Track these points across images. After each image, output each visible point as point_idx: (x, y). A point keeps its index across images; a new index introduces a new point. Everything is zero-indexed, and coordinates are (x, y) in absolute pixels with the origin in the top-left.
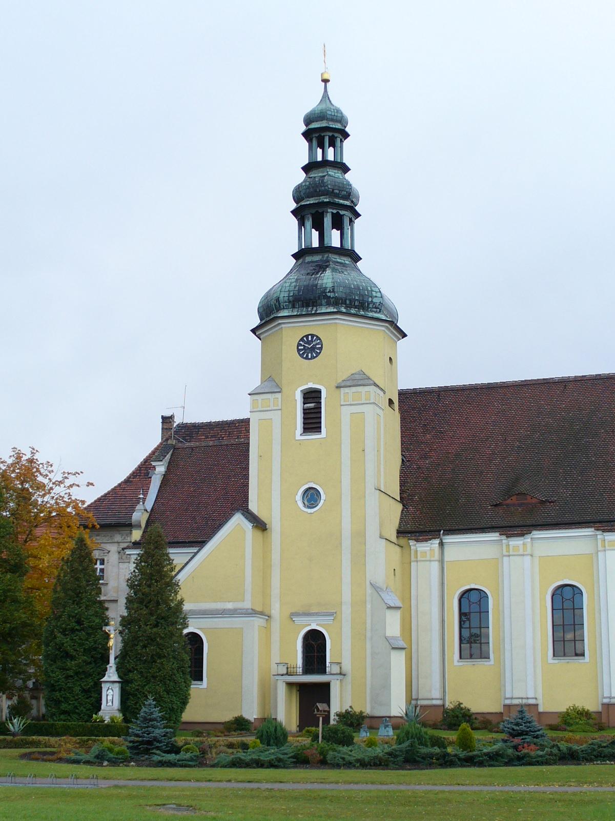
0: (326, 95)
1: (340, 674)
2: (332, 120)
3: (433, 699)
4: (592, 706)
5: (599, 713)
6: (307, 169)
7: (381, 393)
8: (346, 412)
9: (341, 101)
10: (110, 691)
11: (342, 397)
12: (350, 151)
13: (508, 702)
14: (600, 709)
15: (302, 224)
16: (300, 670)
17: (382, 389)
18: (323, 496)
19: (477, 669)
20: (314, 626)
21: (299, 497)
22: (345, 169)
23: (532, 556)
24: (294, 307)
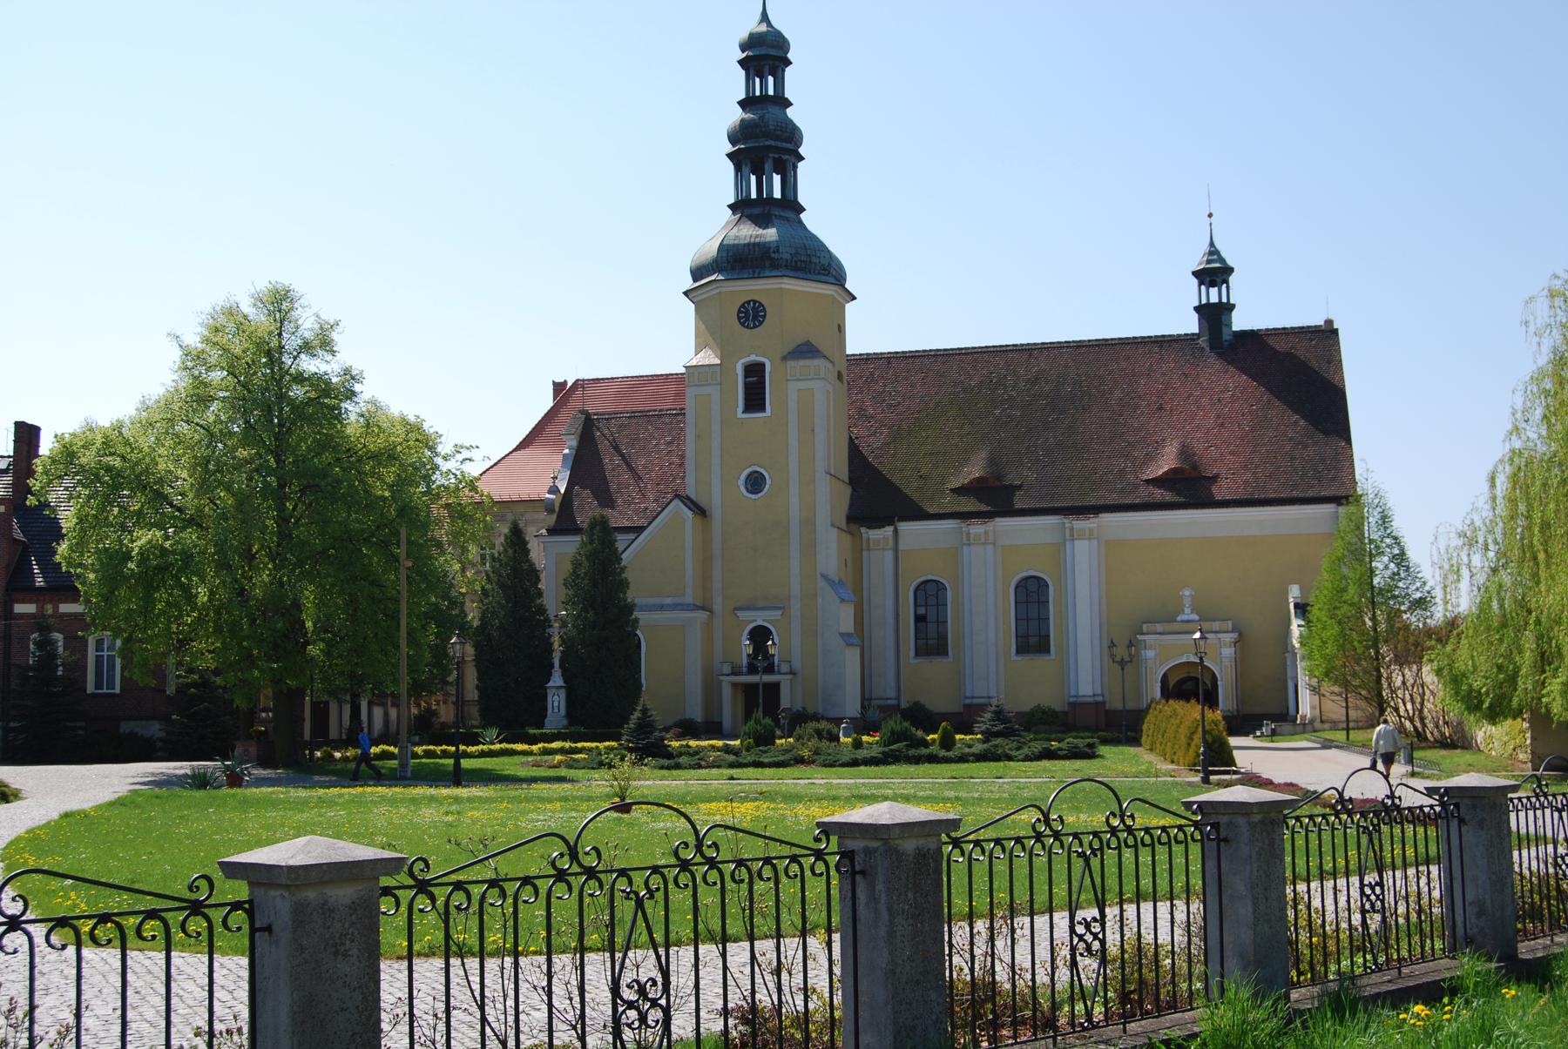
1: (791, 673)
2: (773, 46)
3: (887, 699)
4: (1057, 705)
5: (1065, 713)
7: (830, 366)
8: (793, 387)
10: (556, 697)
12: (795, 82)
14: (1066, 709)
15: (738, 169)
16: (745, 670)
17: (831, 362)
18: (768, 482)
19: (935, 669)
21: (741, 482)
23: (994, 544)
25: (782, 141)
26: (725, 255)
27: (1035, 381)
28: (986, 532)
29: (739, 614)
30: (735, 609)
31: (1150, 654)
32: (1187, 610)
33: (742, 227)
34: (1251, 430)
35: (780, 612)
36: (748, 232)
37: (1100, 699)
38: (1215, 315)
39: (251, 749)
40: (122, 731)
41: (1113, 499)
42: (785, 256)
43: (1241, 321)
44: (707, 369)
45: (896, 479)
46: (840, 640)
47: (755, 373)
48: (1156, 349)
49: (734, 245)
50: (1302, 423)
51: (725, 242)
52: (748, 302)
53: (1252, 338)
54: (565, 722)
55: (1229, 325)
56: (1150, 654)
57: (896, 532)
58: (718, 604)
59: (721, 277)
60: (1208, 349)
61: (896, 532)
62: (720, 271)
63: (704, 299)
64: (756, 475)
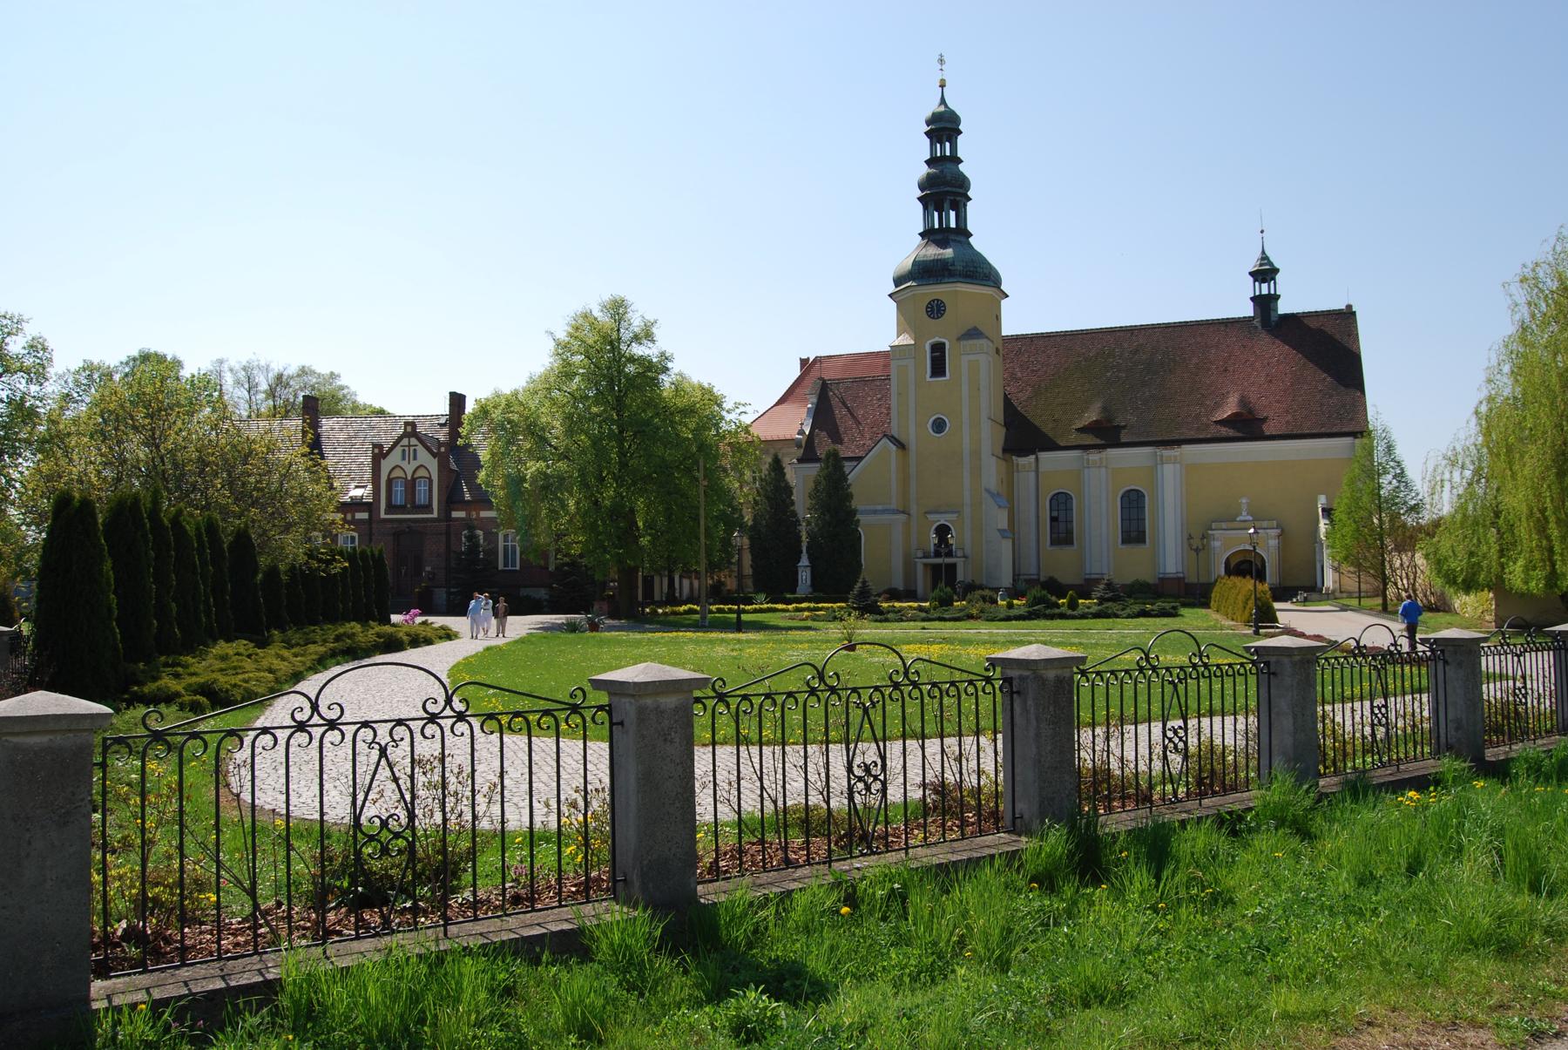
0: (943, 101)
2: (949, 121)
6: (928, 162)
12: (965, 146)
13: (1087, 577)
15: (925, 208)
18: (948, 425)
19: (1065, 554)
20: (942, 522)
21: (929, 425)
27: (1136, 352)
31: (1217, 544)
32: (1244, 513)
35: (956, 515)
36: (933, 252)
41: (1192, 434)
43: (1284, 307)
45: (1037, 423)
47: (938, 349)
50: (1329, 379)
52: (933, 301)
54: (810, 590)
56: (1217, 544)
57: (1037, 459)
58: (914, 510)
61: (1037, 459)
62: (914, 280)
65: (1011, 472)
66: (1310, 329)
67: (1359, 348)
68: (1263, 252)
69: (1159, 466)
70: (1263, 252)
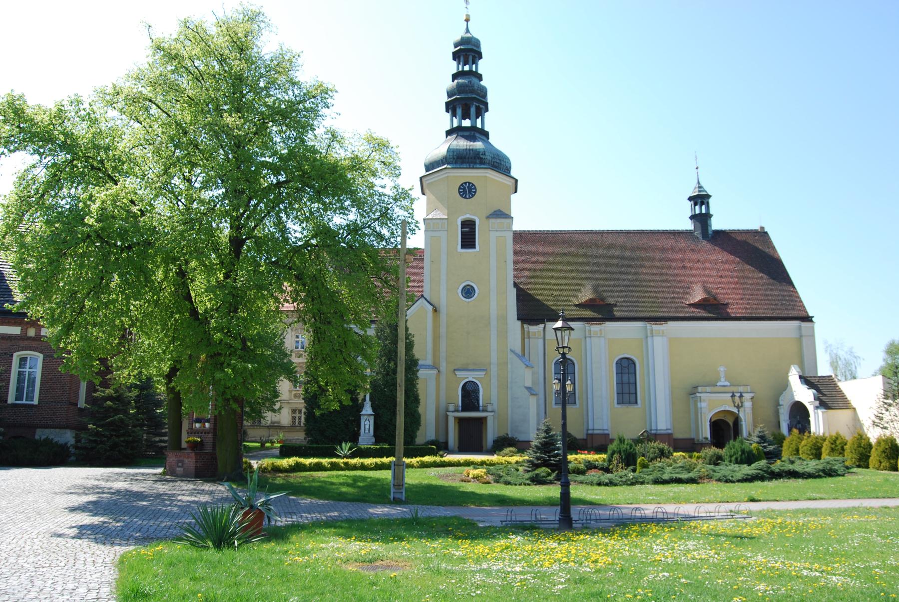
0: (468, 31)
2: (474, 45)
6: (455, 77)
8: (493, 235)
9: (476, 32)
11: (490, 224)
12: (482, 67)
13: (590, 432)
20: (471, 379)
21: (459, 291)
22: (480, 77)
24: (456, 163)
25: (480, 96)
26: (451, 154)
27: (609, 249)
28: (600, 330)
29: (457, 373)
30: (455, 370)
31: (704, 405)
32: (723, 379)
33: (459, 141)
34: (739, 280)
35: (484, 373)
36: (462, 144)
37: (670, 432)
38: (702, 219)
39: (186, 461)
40: (37, 437)
41: (672, 314)
42: (489, 158)
43: (716, 224)
44: (438, 221)
45: (539, 297)
46: (526, 392)
48: (673, 237)
49: (457, 149)
50: (765, 277)
51: (451, 147)
52: (465, 183)
53: (717, 232)
54: (373, 440)
55: (711, 226)
56: (704, 405)
57: (544, 328)
58: (443, 366)
59: (449, 167)
60: (701, 238)
61: (544, 328)
62: (448, 164)
63: (435, 181)
64: (468, 287)
65: (524, 336)
66: (738, 241)
67: (779, 256)
68: (699, 183)
69: (649, 339)
70: (699, 183)
